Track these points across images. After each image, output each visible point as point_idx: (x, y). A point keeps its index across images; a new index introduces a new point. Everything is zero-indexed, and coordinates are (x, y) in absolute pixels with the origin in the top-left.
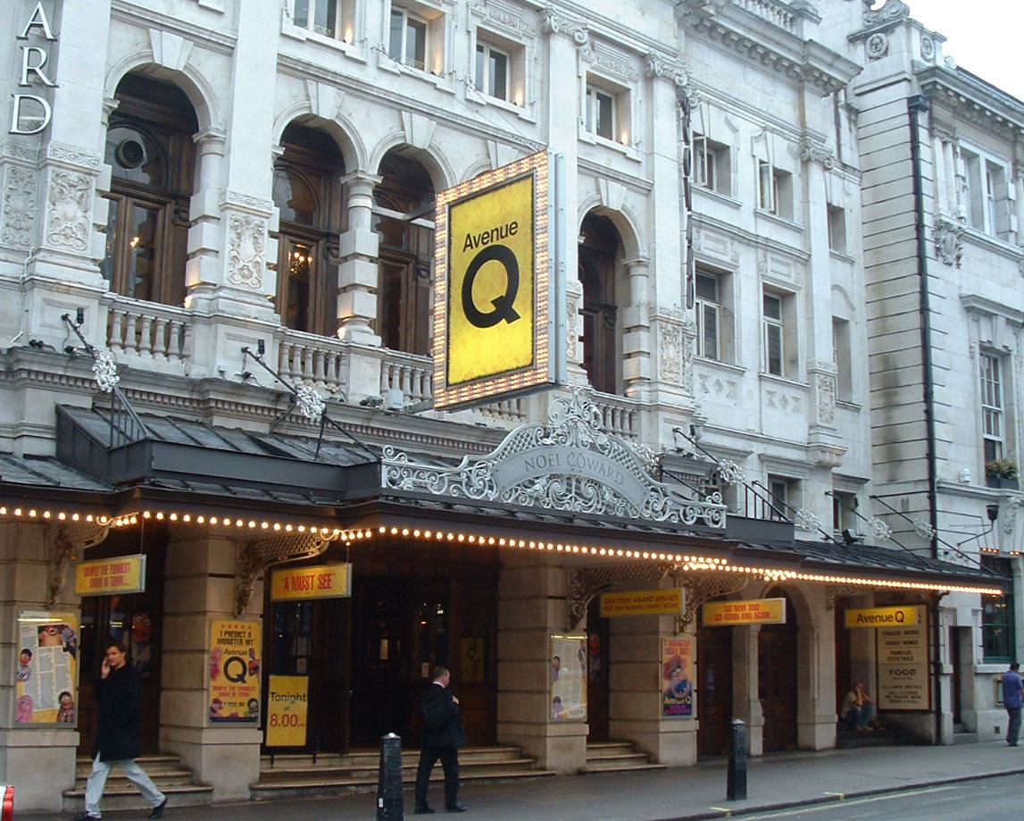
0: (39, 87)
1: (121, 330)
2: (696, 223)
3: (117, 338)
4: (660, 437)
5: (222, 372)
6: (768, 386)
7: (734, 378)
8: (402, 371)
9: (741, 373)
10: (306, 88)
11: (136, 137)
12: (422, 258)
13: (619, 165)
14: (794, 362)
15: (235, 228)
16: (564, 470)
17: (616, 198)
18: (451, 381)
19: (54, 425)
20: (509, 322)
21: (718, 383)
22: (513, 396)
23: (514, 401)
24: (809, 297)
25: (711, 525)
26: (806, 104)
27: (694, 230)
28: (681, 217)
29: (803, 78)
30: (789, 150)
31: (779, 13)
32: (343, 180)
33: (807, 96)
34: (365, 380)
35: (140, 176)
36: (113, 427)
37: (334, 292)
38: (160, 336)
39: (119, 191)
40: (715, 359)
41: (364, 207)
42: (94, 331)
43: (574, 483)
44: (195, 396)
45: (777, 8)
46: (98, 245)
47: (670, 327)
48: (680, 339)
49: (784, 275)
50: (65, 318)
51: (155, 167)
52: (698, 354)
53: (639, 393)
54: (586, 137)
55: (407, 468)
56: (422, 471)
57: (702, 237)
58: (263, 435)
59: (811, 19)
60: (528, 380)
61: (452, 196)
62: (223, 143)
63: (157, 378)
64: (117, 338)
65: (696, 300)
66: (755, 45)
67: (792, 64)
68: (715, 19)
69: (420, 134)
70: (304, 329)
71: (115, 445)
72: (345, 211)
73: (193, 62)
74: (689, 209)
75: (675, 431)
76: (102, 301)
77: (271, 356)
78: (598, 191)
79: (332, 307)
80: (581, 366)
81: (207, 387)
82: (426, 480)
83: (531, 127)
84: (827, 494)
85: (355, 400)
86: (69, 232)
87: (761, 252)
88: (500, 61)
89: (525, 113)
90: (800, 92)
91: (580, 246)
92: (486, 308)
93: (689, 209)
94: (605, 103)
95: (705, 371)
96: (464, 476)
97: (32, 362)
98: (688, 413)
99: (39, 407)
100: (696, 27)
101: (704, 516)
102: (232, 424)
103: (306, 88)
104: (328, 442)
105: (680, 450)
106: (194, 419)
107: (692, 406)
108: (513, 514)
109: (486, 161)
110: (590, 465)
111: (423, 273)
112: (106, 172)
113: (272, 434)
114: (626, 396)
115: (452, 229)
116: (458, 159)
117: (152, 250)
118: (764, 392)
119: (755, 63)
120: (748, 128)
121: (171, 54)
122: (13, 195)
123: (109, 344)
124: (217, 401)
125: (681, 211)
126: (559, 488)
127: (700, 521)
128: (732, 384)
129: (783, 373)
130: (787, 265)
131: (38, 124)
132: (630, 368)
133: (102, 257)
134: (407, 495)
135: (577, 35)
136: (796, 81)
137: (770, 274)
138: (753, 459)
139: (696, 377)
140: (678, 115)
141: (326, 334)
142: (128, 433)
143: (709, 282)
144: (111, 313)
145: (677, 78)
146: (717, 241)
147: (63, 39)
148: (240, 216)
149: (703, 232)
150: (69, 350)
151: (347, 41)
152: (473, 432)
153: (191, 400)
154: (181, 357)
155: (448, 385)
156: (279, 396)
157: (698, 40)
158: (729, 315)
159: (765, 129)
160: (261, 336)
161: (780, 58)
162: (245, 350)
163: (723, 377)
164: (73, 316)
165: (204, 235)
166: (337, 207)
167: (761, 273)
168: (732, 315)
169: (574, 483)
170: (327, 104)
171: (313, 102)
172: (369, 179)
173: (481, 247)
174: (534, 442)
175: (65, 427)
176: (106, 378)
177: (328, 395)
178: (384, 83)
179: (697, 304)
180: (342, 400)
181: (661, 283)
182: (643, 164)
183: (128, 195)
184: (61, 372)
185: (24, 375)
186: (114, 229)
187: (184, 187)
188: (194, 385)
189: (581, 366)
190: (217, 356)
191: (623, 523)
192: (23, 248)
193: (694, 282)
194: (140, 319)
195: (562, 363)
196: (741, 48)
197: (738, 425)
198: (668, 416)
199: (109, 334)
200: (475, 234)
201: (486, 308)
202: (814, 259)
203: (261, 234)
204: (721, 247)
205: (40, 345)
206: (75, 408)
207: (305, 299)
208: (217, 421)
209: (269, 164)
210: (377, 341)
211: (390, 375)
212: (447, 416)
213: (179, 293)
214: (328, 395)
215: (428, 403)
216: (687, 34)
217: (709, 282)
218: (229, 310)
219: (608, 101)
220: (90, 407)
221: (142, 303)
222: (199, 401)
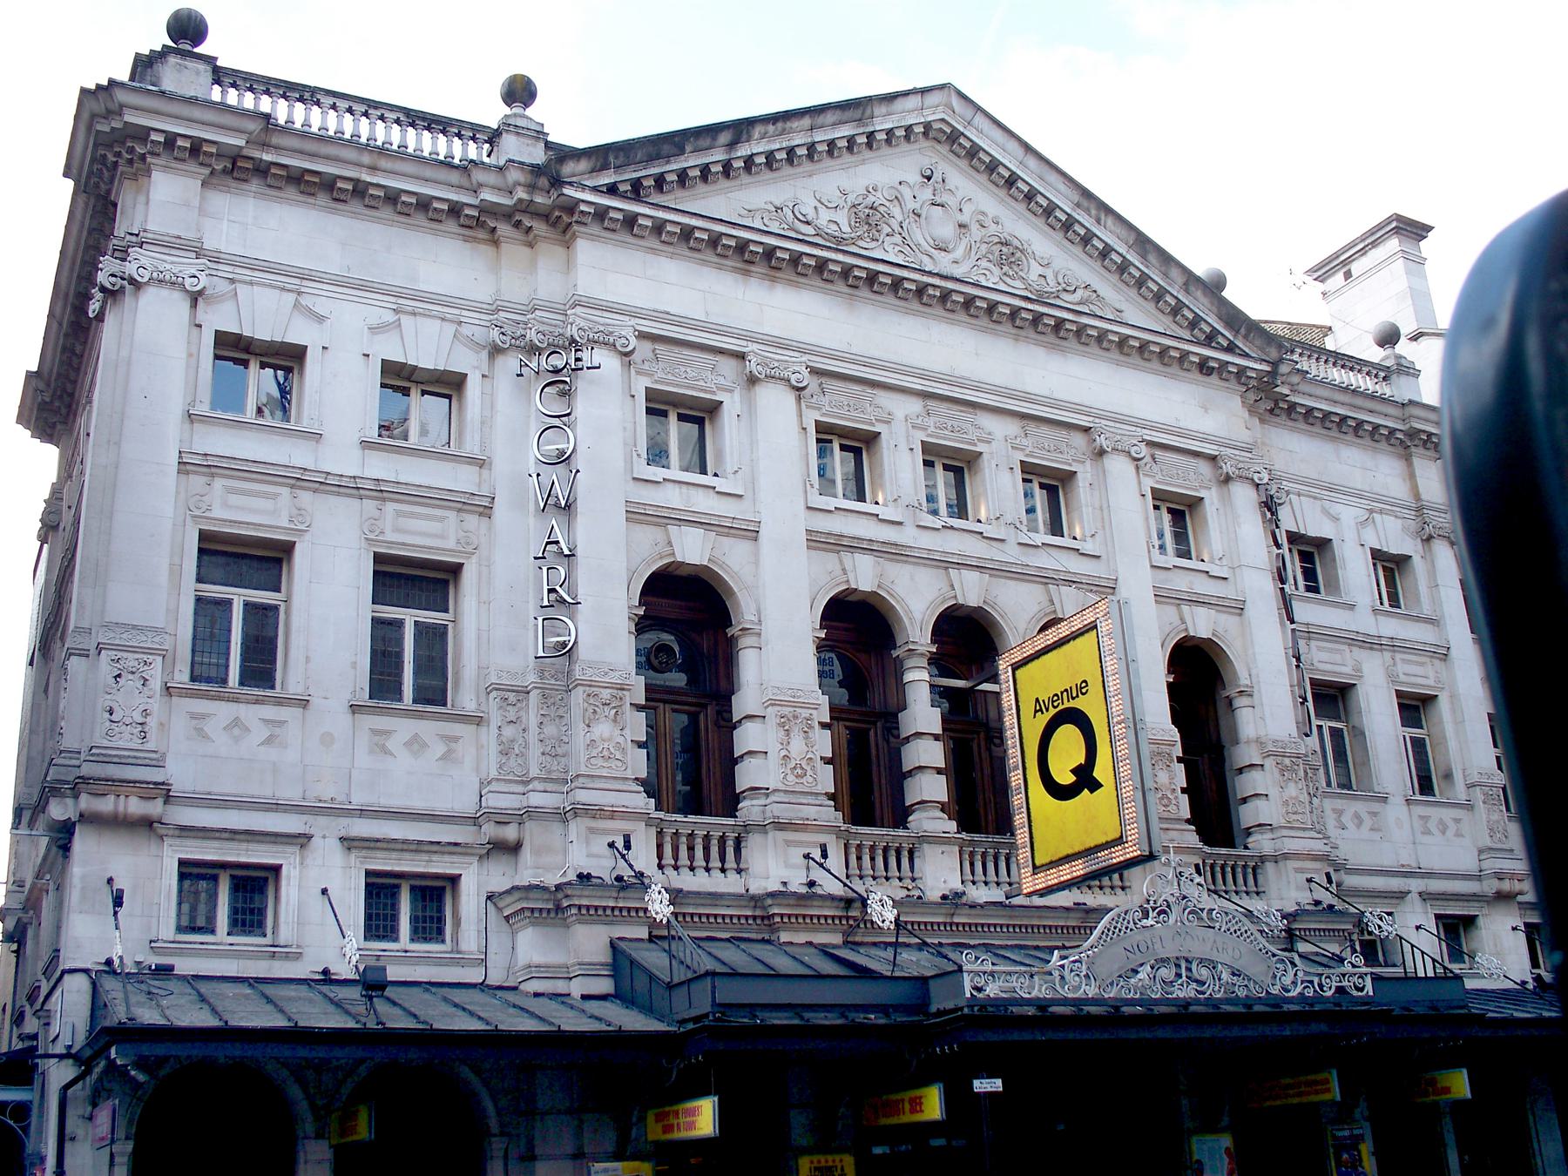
0: (560, 603)
1: (669, 849)
2: (1299, 638)
3: (668, 859)
4: (1287, 891)
5: (785, 884)
6: (1419, 810)
7: (1376, 807)
8: (984, 855)
9: (1385, 800)
10: (841, 562)
11: (668, 638)
12: (993, 724)
13: (1203, 587)
14: (1448, 776)
15: (782, 725)
16: (1169, 951)
17: (1202, 625)
18: (1038, 863)
19: (610, 960)
20: (1092, 791)
21: (1357, 816)
22: (1114, 871)
23: (1116, 876)
24: (1453, 697)
25: (1355, 993)
26: (1418, 472)
27: (1302, 643)
28: (1284, 632)
29: (140, 150)
30: (1404, 528)
31: (1368, 374)
32: (895, 654)
33: (1416, 461)
34: (940, 872)
35: (678, 679)
36: (672, 956)
37: (899, 777)
38: (714, 850)
39: (655, 697)
40: (1350, 788)
41: (919, 679)
42: (643, 857)
43: (1183, 965)
44: (758, 913)
45: (1365, 369)
46: (638, 763)
47: (1287, 761)
48: (1302, 773)
49: (1420, 677)
50: (611, 845)
51: (690, 666)
52: (1329, 784)
53: (1262, 843)
54: (1160, 560)
55: (992, 974)
56: (1010, 974)
57: (1314, 649)
58: (835, 947)
59: (1408, 374)
60: (1118, 855)
61: (1017, 656)
62: (759, 635)
63: (715, 897)
64: (668, 859)
65: (1315, 722)
66: (1344, 419)
67: (1392, 431)
68: (1292, 399)
69: (971, 591)
70: (871, 823)
71: (676, 980)
72: (901, 687)
73: (717, 553)
74: (1292, 622)
75: (1310, 880)
76: (649, 822)
77: (835, 861)
78: (1183, 621)
79: (899, 793)
80: (1188, 821)
81: (769, 901)
82: (1015, 983)
83: (1094, 561)
84: (1514, 929)
85: (934, 895)
86: (606, 753)
87: (1387, 655)
88: (1052, 492)
89: (1088, 547)
90: (1408, 459)
91: (1169, 685)
92: (1065, 778)
93: (1292, 622)
94: (1178, 516)
95: (1339, 803)
96: (1056, 974)
97: (580, 896)
98: (1324, 858)
99: (591, 942)
100: (1271, 411)
101: (1345, 983)
102: (801, 938)
103: (841, 562)
104: (908, 945)
105: (1317, 903)
106: (760, 937)
107: (1327, 848)
108: (1117, 1008)
109: (1052, 608)
110: (1200, 943)
111: (997, 741)
112: (638, 684)
113: (846, 943)
114: (1246, 848)
115: (1022, 693)
116: (1016, 611)
117: (695, 767)
118: (1415, 818)
119: (1348, 437)
120: (1350, 514)
121: (692, 549)
122: (545, 720)
123: (660, 867)
124: (782, 916)
125: (1282, 625)
126: (1166, 973)
127: (1341, 990)
128: (1375, 814)
129: (1437, 791)
130: (1422, 664)
131: (564, 645)
132: (1247, 815)
133: (644, 775)
134: (996, 1002)
135: (1133, 450)
136: (1401, 450)
137: (1402, 678)
138: (1414, 896)
139: (1328, 812)
140: (1264, 515)
141: (896, 826)
142: (688, 961)
143: (1331, 698)
144: (660, 833)
145: (1256, 477)
146: (1331, 651)
147: (579, 552)
148: (786, 711)
149: (1313, 643)
150: (619, 879)
151: (883, 502)
152: (1072, 915)
153: (755, 918)
154: (739, 871)
155: (1035, 867)
156: (848, 903)
157: (1277, 425)
158: (1359, 733)
159: (1371, 511)
160: (823, 838)
161: (1376, 427)
162: (807, 856)
163: (1361, 807)
164: (620, 844)
165: (747, 738)
166: (891, 681)
167: (1392, 678)
168: (1363, 734)
169: (1183, 965)
170: (864, 576)
171: (1058, 606)
172: (922, 649)
173: (1052, 711)
174: (1131, 925)
175: (620, 960)
176: (659, 907)
177: (904, 893)
178: (926, 541)
179: (1320, 727)
180: (920, 898)
181: (1267, 713)
182: (1231, 579)
183: (665, 702)
184: (612, 904)
185: (574, 911)
186: (653, 743)
187: (723, 684)
188: (756, 900)
189: (1188, 821)
190: (773, 867)
191: (1248, 1003)
192: (563, 776)
193: (1310, 704)
194: (691, 836)
195: (1155, 825)
196: (1328, 424)
197: (1387, 862)
198: (1298, 864)
199: (660, 856)
200: (1044, 697)
201: (1065, 778)
202: (1453, 652)
203: (811, 727)
204: (1337, 658)
205: (589, 876)
206: (631, 940)
207: (868, 785)
208: (785, 937)
209: (812, 649)
210: (952, 826)
211: (968, 858)
212: (1037, 901)
213: (730, 802)
214: (904, 893)
215: (1014, 889)
216: (1262, 421)
217: (1331, 698)
218: (786, 815)
219: (1180, 512)
220: (646, 936)
221: (691, 818)
222: (763, 918)
